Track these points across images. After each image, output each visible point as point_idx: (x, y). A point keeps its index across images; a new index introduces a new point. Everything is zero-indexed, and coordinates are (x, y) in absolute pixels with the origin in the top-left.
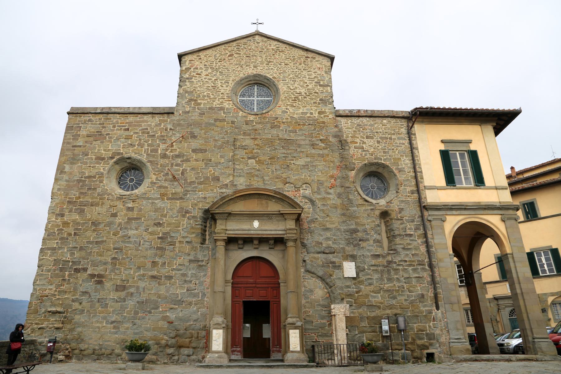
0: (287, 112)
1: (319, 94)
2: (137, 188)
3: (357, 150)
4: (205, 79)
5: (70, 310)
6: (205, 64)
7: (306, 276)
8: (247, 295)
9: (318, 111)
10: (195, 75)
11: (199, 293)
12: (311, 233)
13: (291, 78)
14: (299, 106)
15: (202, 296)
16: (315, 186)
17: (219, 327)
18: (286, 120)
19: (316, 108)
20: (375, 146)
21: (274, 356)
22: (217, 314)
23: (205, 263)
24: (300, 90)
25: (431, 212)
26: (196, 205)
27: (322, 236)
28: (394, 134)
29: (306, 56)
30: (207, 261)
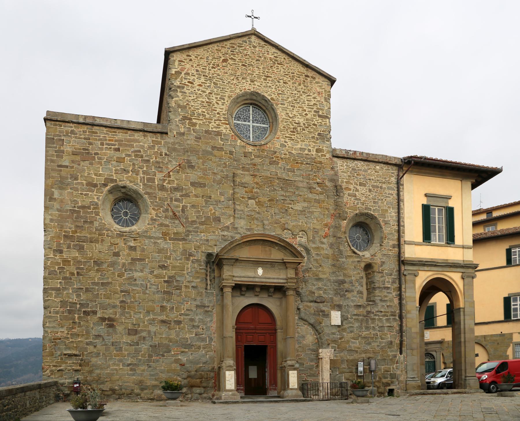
1: (318, 127)
3: (350, 197)
9: (316, 148)
10: (187, 83)
12: (305, 282)
14: (298, 139)
15: (209, 341)
17: (231, 369)
18: (284, 156)
19: (314, 144)
21: (271, 393)
22: (228, 357)
23: (211, 308)
26: (199, 247)
27: (314, 286)
28: (384, 183)
29: (306, 74)
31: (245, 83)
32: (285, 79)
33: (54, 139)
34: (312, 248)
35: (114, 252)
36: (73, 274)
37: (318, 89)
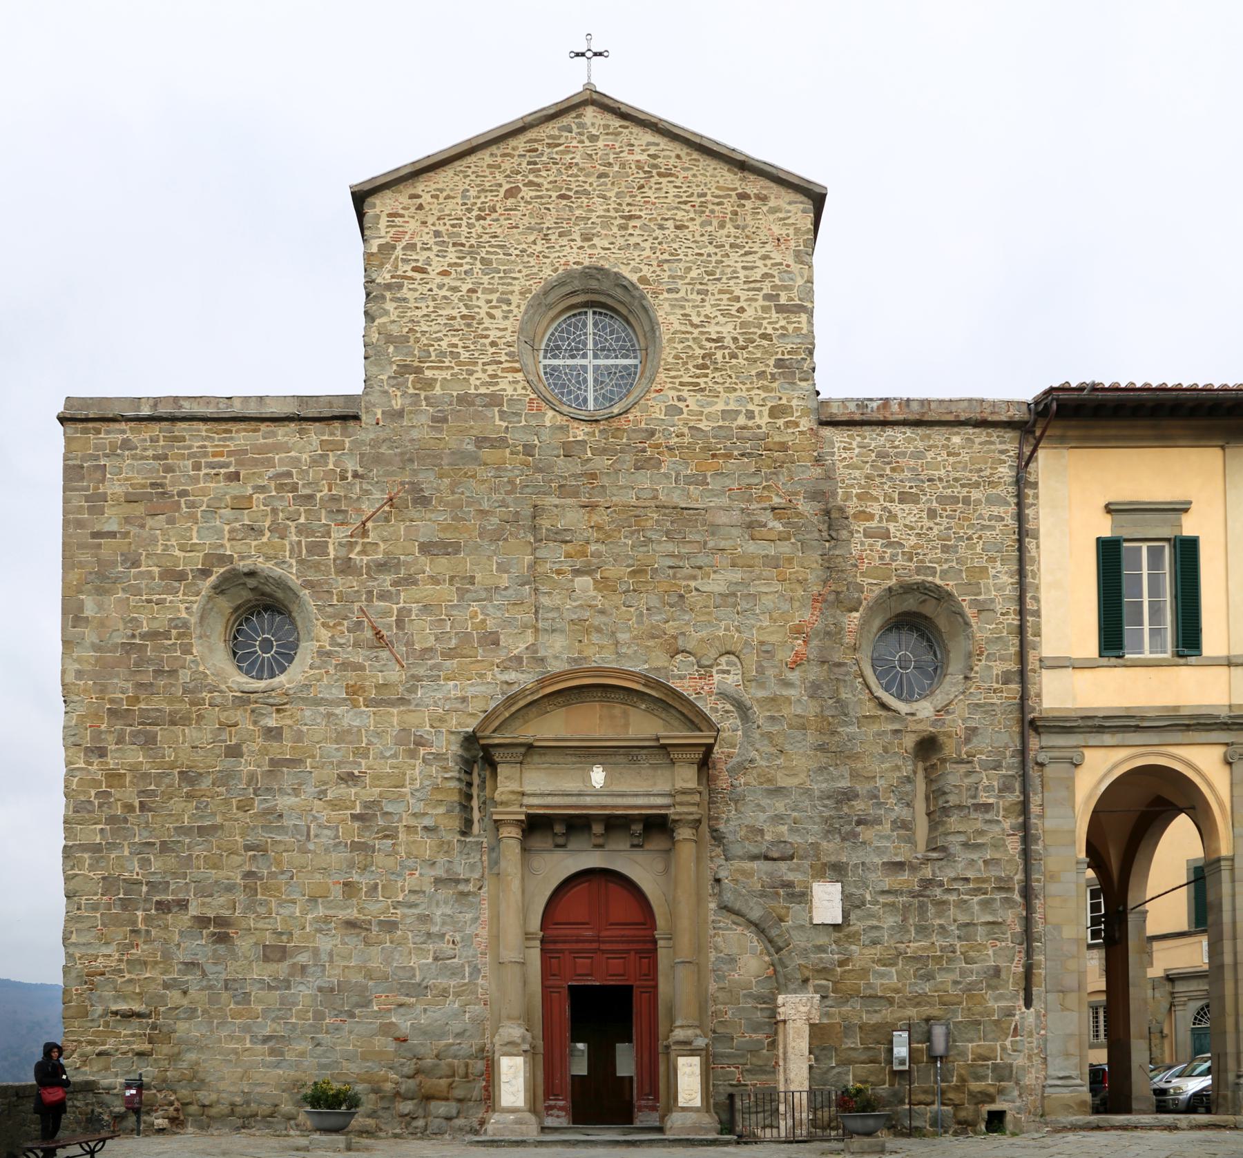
1: (775, 341)
4: (441, 287)
5: (162, 1009)
7: (720, 921)
9: (770, 404)
10: (410, 274)
11: (463, 966)
12: (736, 802)
14: (716, 386)
15: (471, 974)
16: (751, 659)
17: (514, 1050)
18: (676, 440)
19: (764, 395)
20: (922, 527)
21: (642, 1119)
22: (509, 1018)
23: (474, 886)
24: (719, 329)
28: (977, 485)
29: (740, 191)
30: (479, 880)
31: (568, 248)
33: (82, 467)
34: (757, 700)
35: (228, 747)
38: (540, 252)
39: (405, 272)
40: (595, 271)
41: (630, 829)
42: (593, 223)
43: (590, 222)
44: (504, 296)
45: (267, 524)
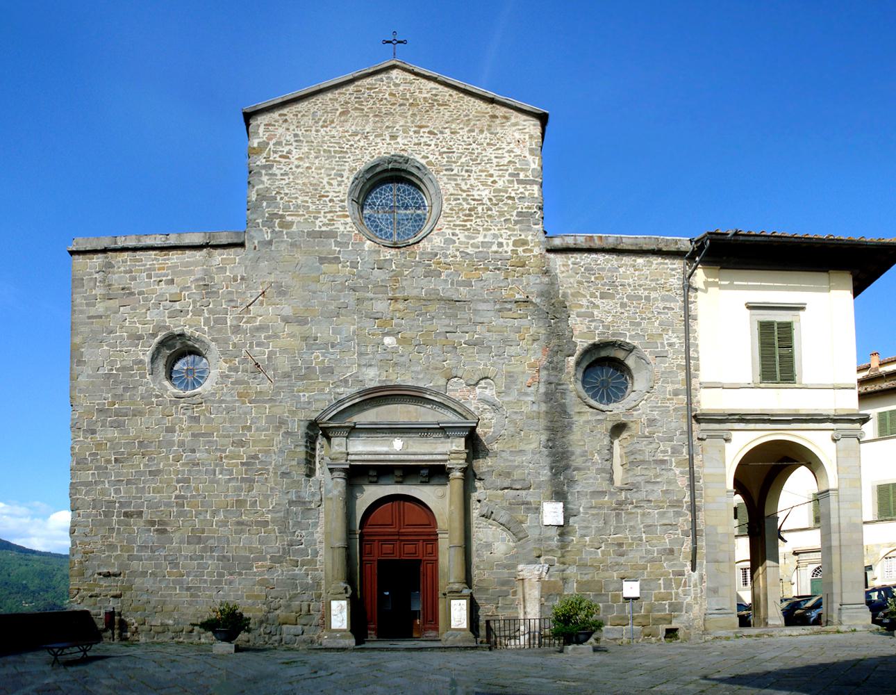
0: (454, 242)
1: (517, 201)
2: (200, 384)
3: (581, 319)
4: (298, 167)
5: (127, 572)
6: (296, 132)
7: (480, 524)
8: (384, 552)
9: (513, 239)
10: (278, 159)
13: (462, 165)
14: (478, 227)
16: (502, 381)
18: (451, 259)
19: (509, 233)
20: (617, 312)
24: (479, 193)
25: (703, 426)
28: (655, 289)
29: (491, 114)
31: (381, 144)
32: (453, 126)
33: (83, 279)
35: (167, 427)
36: (108, 461)
37: (517, 135)
38: (362, 147)
39: (275, 158)
40: (398, 158)
41: (420, 473)
42: (397, 130)
43: (395, 129)
44: (339, 172)
45: (190, 308)
